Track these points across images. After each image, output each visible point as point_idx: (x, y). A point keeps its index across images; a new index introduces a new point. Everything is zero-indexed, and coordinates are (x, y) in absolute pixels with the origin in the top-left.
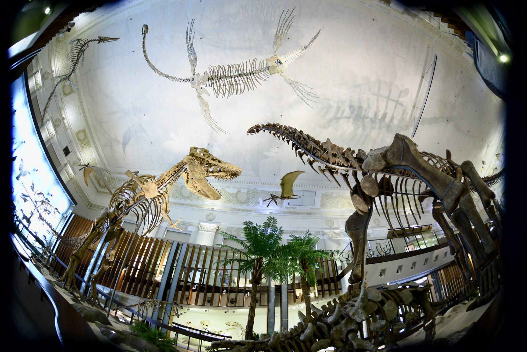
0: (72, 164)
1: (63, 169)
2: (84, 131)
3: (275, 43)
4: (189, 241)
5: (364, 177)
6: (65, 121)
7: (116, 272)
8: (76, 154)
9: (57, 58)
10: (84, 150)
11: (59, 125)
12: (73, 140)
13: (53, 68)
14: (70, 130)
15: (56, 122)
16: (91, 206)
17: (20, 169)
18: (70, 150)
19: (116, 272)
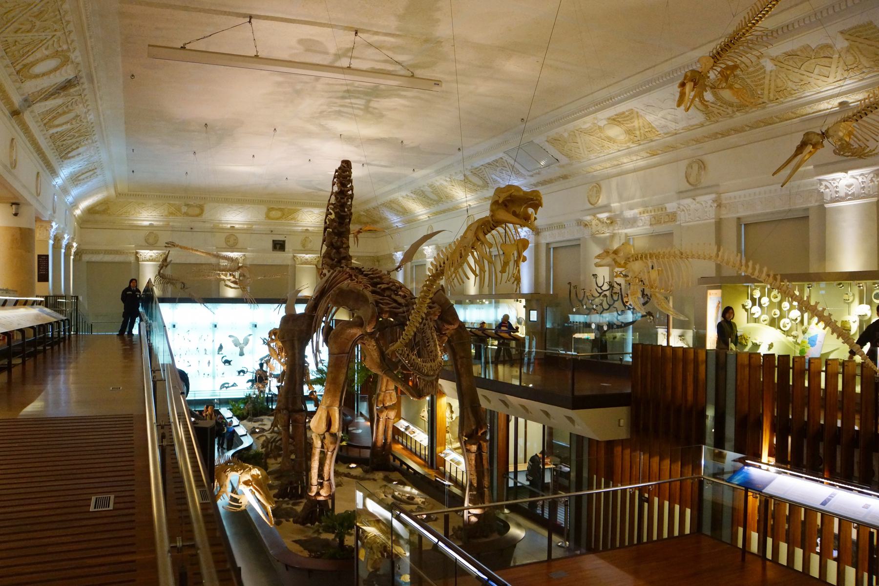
0: (303, 249)
1: (295, 267)
2: (270, 209)
3: (829, 500)
4: (809, 270)
5: (178, 373)
6: (237, 226)
7: (603, 479)
8: (294, 233)
9: (133, 215)
10: (299, 218)
11: (236, 239)
12: (272, 228)
13: (147, 223)
14: (255, 225)
15: (228, 244)
16: (378, 261)
17: (236, 346)
18: (281, 238)
19: (603, 479)
